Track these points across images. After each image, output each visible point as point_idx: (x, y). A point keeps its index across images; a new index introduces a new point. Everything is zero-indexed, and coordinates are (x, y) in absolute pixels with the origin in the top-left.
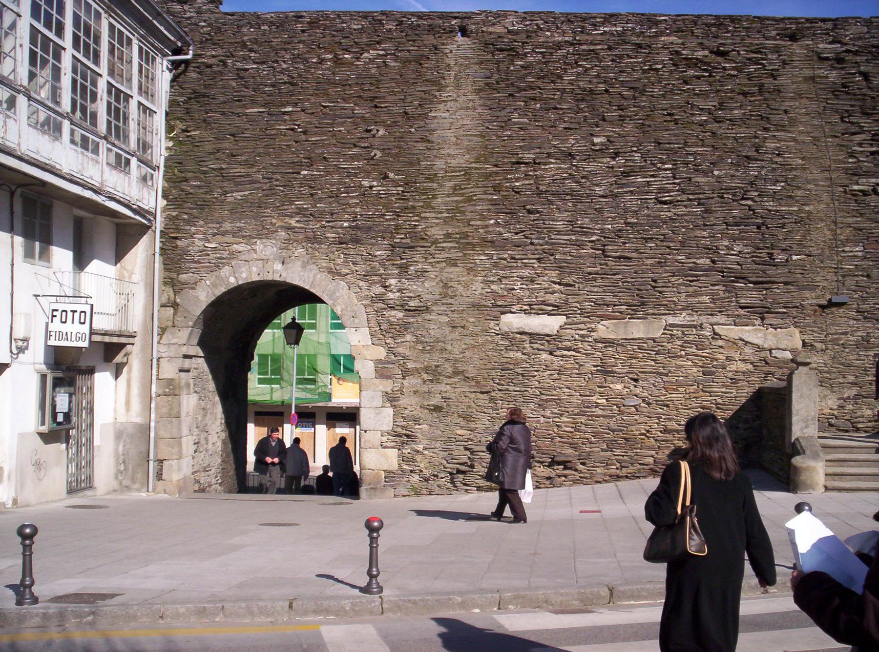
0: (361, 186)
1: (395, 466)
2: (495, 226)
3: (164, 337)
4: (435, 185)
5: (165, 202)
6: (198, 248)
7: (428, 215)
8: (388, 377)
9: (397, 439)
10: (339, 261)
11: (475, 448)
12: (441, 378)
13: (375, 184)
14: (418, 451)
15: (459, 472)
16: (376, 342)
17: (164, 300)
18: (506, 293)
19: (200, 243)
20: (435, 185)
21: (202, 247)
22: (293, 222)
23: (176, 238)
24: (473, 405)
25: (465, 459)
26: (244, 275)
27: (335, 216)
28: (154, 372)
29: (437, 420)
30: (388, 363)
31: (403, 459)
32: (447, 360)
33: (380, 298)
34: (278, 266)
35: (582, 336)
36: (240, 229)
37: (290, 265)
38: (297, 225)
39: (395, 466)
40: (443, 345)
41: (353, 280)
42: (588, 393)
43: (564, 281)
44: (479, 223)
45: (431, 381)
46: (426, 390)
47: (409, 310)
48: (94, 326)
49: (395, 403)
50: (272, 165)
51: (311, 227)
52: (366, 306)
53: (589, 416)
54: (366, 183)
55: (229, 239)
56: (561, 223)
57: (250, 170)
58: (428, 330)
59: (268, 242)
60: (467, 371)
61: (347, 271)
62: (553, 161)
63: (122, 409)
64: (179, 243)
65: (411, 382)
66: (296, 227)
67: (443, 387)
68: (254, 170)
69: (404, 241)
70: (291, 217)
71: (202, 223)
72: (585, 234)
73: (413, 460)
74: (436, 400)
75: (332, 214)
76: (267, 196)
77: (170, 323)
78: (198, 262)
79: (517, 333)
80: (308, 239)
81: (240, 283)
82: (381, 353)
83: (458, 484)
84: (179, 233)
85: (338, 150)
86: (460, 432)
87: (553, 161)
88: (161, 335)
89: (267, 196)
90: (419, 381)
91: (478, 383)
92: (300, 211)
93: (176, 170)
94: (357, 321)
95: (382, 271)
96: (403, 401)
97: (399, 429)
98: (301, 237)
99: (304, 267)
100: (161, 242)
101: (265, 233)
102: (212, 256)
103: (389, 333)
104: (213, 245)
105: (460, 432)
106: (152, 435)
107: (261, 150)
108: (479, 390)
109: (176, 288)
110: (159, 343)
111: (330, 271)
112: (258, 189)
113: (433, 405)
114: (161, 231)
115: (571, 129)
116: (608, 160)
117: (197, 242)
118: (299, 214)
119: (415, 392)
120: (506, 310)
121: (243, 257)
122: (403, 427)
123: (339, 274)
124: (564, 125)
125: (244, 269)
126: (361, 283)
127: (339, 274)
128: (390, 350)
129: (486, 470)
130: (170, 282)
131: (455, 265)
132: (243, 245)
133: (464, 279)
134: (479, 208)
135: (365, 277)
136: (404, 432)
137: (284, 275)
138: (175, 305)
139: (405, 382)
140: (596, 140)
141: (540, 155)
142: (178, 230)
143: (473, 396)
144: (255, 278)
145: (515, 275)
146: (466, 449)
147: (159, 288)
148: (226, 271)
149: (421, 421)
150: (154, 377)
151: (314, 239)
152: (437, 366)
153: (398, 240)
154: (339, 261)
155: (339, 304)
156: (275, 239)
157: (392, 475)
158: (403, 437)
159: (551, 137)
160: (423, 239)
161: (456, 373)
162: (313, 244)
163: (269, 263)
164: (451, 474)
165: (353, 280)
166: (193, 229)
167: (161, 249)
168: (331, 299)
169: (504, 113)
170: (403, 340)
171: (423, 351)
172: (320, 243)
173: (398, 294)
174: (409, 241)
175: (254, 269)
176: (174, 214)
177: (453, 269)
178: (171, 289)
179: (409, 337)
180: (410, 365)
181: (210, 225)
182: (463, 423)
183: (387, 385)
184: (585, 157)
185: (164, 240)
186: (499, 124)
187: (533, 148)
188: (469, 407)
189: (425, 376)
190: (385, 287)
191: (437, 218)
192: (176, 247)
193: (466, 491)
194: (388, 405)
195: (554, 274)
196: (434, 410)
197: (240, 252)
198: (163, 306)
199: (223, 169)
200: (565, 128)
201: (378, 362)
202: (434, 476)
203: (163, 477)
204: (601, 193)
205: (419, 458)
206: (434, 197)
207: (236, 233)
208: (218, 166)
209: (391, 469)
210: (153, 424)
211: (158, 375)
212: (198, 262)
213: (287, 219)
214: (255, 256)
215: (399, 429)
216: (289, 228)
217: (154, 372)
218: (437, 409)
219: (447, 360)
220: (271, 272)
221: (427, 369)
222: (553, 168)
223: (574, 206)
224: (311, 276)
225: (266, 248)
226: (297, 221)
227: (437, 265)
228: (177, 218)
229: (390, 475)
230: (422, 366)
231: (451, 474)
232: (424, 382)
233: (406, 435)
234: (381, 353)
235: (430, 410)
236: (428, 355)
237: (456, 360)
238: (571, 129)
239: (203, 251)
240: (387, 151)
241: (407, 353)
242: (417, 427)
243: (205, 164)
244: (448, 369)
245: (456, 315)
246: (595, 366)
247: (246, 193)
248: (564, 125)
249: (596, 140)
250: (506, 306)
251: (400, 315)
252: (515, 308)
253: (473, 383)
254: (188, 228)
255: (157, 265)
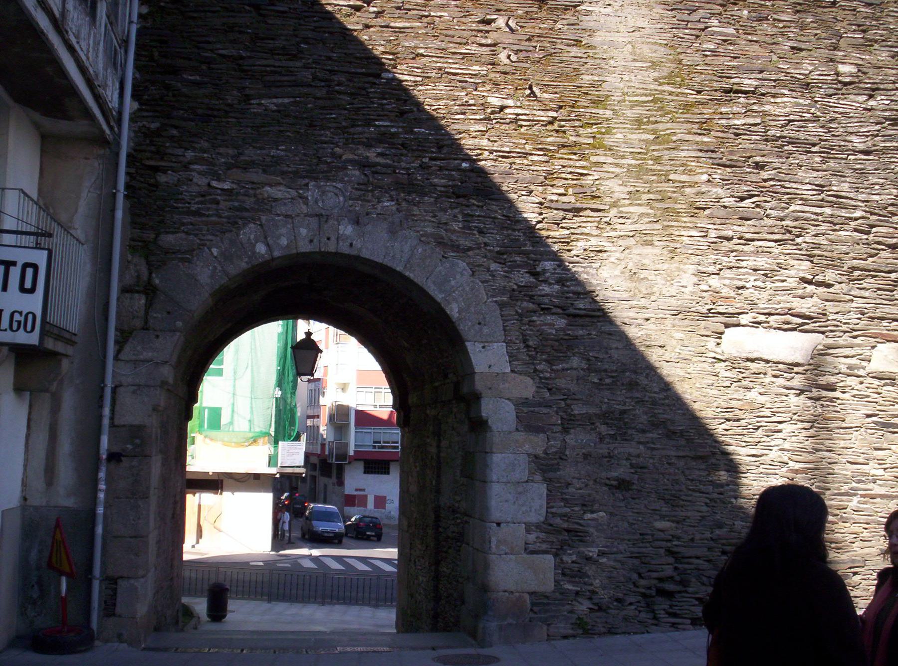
0: (485, 106)
1: (549, 586)
2: (706, 182)
3: (127, 348)
4: (608, 114)
5: (136, 105)
6: (196, 189)
7: (602, 159)
8: (538, 430)
9: (552, 538)
10: (456, 226)
11: (685, 551)
12: (630, 432)
13: (510, 102)
14: (588, 559)
15: (661, 592)
16: (519, 369)
17: (129, 280)
18: (732, 294)
19: (203, 181)
20: (608, 114)
21: (206, 188)
22: (371, 155)
23: (156, 169)
24: (682, 479)
25: (669, 571)
26: (284, 242)
27: (445, 150)
28: (107, 411)
29: (622, 504)
30: (540, 405)
31: (564, 572)
32: (640, 401)
33: (526, 292)
34: (347, 229)
35: (850, 367)
36: (277, 161)
37: (369, 227)
38: (380, 160)
39: (549, 586)
40: (633, 376)
41: (480, 260)
42: (861, 460)
43: (820, 278)
44: (684, 178)
45: (613, 437)
46: (605, 451)
47: (575, 316)
48: (116, 422)
49: (551, 475)
50: (330, 58)
51: (403, 164)
52: (502, 305)
53: (862, 496)
54: (495, 101)
55: (256, 176)
56: (809, 187)
57: (291, 64)
58: (607, 349)
59: (329, 186)
60: (673, 422)
61: (468, 244)
62: (786, 92)
63: (38, 483)
64: (162, 178)
65: (578, 439)
66: (379, 164)
67: (632, 449)
68: (299, 64)
69: (564, 199)
70: (369, 146)
71: (206, 145)
72: (842, 207)
73: (581, 574)
74: (621, 471)
75: (440, 148)
76: (323, 108)
77: (138, 323)
78: (197, 213)
79: (748, 360)
80: (399, 186)
81: (276, 254)
82: (526, 388)
83: (662, 614)
84: (162, 159)
85: (443, 45)
86: (659, 525)
87: (786, 92)
88: (120, 344)
89: (323, 108)
90: (593, 437)
91: (689, 441)
92: (384, 138)
93: (156, 54)
94: (486, 330)
95: (528, 248)
96: (568, 471)
97: (558, 521)
98: (387, 180)
99: (392, 232)
100: (127, 174)
101: (320, 170)
102: (223, 205)
103: (543, 353)
104: (226, 186)
105: (659, 525)
106: (99, 530)
107: (310, 34)
108: (692, 454)
109: (152, 258)
110: (116, 358)
111: (440, 242)
112: (307, 95)
113: (617, 479)
114: (129, 156)
115: (801, 50)
116: (865, 98)
117: (63, 217)
118: (381, 142)
119: (586, 456)
120: (731, 321)
121: (282, 209)
122: (562, 516)
123: (456, 248)
124: (791, 43)
125: (283, 231)
126: (493, 266)
127: (456, 248)
128: (545, 384)
129: (710, 590)
130: (142, 246)
131: (650, 244)
132: (282, 188)
133: (665, 266)
134: (683, 154)
135: (499, 257)
136: (565, 525)
137: (357, 244)
138: (150, 291)
139: (568, 438)
140: (842, 68)
141: (765, 83)
142: (160, 154)
143: (681, 463)
144: (304, 247)
145: (743, 264)
146: (670, 552)
147: (122, 255)
148: (249, 232)
149: (596, 507)
150: (106, 422)
151: (409, 187)
152: (623, 412)
153: (555, 198)
154: (456, 226)
155: (455, 300)
156: (342, 181)
157: (545, 601)
158: (560, 534)
159: (775, 58)
160: (594, 197)
161: (655, 424)
162: (409, 193)
163: (331, 222)
164: (644, 595)
165: (480, 260)
166: (190, 154)
167: (128, 186)
168: (441, 291)
169: (695, 17)
170: (565, 366)
171: (599, 386)
172: (423, 194)
173: (557, 287)
174: (572, 199)
175: (303, 231)
176: (153, 126)
177: (649, 250)
178: (143, 261)
179: (575, 362)
180: (578, 409)
181: (222, 150)
182: (665, 509)
183: (537, 443)
184: (831, 91)
185: (133, 171)
186: (693, 32)
187: (752, 71)
188: (677, 482)
189: (603, 429)
190: (535, 274)
191: (617, 165)
192: (156, 185)
193: (673, 625)
194: (538, 477)
195: (804, 268)
196: (617, 488)
197: (276, 200)
198: (125, 290)
199: (242, 58)
200: (793, 48)
201: (521, 404)
202: (619, 600)
203: (118, 610)
204: (861, 147)
205: (590, 570)
206: (608, 131)
207: (270, 166)
208: (234, 52)
209: (541, 589)
210: (100, 510)
211: (112, 418)
212: (197, 213)
213: (361, 150)
214: (305, 209)
215: (558, 521)
216: (364, 165)
217: (107, 411)
218: (622, 485)
219: (640, 401)
220: (333, 239)
221: (606, 417)
222: (786, 105)
223: (824, 162)
224: (407, 249)
225: (329, 196)
226: (379, 155)
227: (621, 242)
228: (157, 133)
229: (540, 601)
230: (596, 411)
231: (644, 595)
232: (601, 439)
233: (568, 531)
234: (526, 388)
235: (611, 487)
236: (607, 393)
237: (654, 403)
238: (801, 50)
239: (206, 194)
240: (524, 54)
241: (573, 388)
242: (588, 516)
243: (210, 47)
244: (641, 416)
245: (652, 327)
246: (868, 416)
247: (286, 101)
248: (791, 43)
249: (842, 68)
250: (732, 315)
251: (561, 322)
252: (744, 319)
253: (683, 442)
254: (179, 152)
255: (119, 214)
